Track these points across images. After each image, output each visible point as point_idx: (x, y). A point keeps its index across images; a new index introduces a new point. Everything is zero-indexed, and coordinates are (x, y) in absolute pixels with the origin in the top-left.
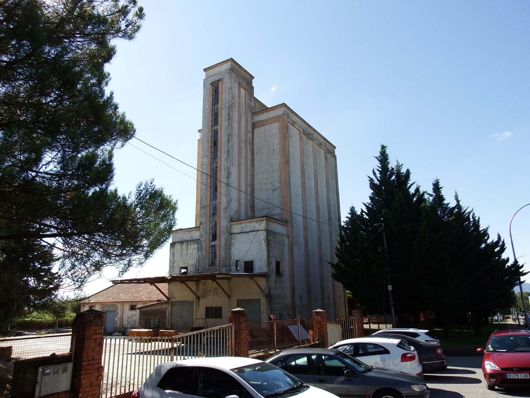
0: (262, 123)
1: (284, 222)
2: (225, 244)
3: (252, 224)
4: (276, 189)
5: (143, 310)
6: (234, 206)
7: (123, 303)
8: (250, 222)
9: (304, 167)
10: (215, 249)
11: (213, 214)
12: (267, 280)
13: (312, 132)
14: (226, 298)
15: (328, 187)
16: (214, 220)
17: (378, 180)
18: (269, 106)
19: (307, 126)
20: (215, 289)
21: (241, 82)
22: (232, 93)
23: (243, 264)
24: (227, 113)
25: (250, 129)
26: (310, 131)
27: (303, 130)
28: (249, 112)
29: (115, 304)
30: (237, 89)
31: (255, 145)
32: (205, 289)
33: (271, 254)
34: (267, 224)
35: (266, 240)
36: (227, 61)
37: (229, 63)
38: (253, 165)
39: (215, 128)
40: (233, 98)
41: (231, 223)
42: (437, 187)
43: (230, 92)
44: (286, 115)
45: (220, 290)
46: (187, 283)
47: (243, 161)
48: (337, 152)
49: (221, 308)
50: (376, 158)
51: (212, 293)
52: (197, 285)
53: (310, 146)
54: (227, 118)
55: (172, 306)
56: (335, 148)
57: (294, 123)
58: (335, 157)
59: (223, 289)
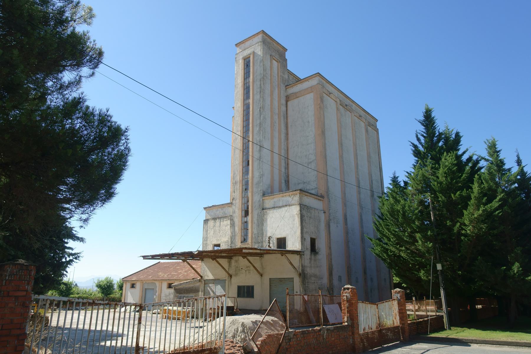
0: (296, 95)
1: (320, 197)
2: (258, 220)
3: (285, 198)
4: (311, 162)
5: (177, 288)
6: (267, 180)
7: (162, 280)
8: (283, 196)
9: (341, 140)
10: (247, 225)
11: (246, 189)
12: (301, 257)
13: (351, 103)
14: (258, 276)
15: (369, 162)
16: (246, 196)
17: (422, 146)
18: (302, 78)
19: (344, 98)
20: (247, 267)
21: (273, 54)
22: (264, 65)
23: (275, 242)
24: (259, 86)
25: (283, 102)
26: (348, 102)
27: (340, 101)
28: (282, 85)
29: (154, 282)
30: (269, 60)
31: (289, 118)
32: (237, 267)
33: (305, 230)
34: (301, 198)
35: (299, 215)
36: (258, 34)
37: (260, 36)
38: (287, 139)
39: (247, 102)
40: (265, 70)
41: (264, 198)
42: (493, 149)
43: (262, 64)
44: (323, 86)
45: (252, 268)
46: (218, 259)
47: (276, 134)
48: (379, 125)
49: (253, 287)
50: (420, 122)
51: (244, 271)
52: (230, 263)
53: (348, 118)
54: (259, 90)
55: (205, 284)
56: (377, 120)
57: (329, 94)
58: (377, 131)
59: (254, 267)
